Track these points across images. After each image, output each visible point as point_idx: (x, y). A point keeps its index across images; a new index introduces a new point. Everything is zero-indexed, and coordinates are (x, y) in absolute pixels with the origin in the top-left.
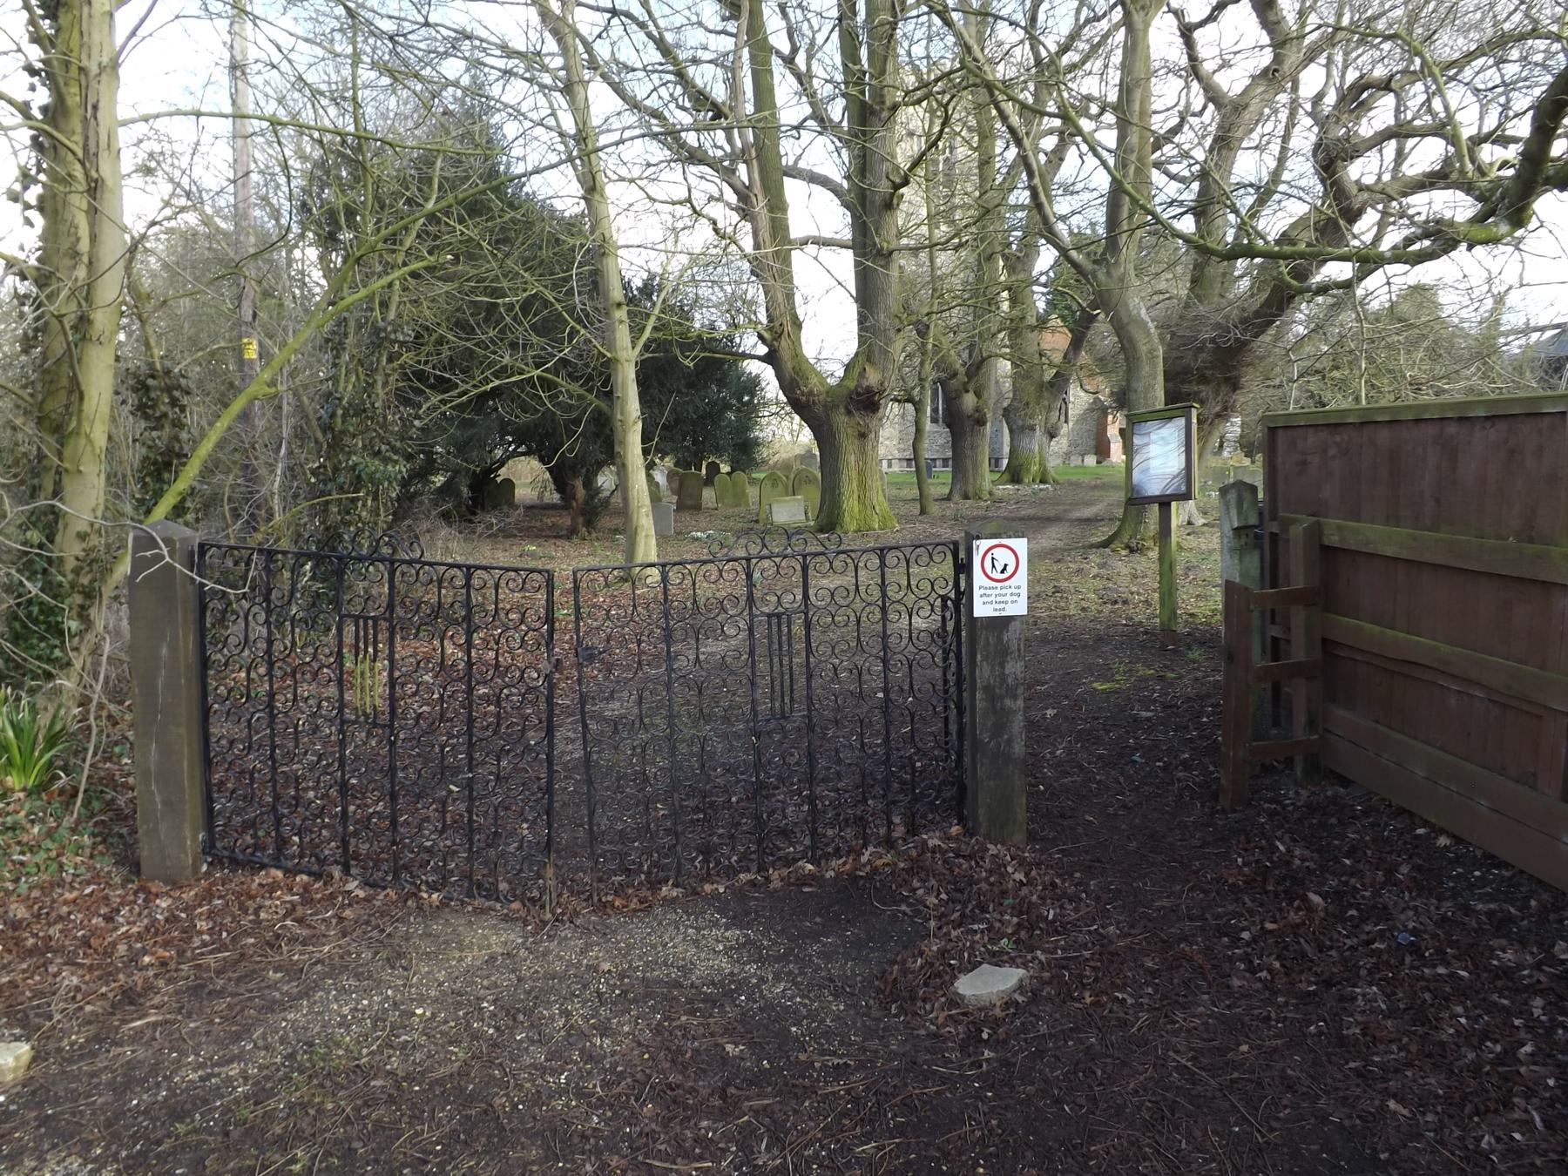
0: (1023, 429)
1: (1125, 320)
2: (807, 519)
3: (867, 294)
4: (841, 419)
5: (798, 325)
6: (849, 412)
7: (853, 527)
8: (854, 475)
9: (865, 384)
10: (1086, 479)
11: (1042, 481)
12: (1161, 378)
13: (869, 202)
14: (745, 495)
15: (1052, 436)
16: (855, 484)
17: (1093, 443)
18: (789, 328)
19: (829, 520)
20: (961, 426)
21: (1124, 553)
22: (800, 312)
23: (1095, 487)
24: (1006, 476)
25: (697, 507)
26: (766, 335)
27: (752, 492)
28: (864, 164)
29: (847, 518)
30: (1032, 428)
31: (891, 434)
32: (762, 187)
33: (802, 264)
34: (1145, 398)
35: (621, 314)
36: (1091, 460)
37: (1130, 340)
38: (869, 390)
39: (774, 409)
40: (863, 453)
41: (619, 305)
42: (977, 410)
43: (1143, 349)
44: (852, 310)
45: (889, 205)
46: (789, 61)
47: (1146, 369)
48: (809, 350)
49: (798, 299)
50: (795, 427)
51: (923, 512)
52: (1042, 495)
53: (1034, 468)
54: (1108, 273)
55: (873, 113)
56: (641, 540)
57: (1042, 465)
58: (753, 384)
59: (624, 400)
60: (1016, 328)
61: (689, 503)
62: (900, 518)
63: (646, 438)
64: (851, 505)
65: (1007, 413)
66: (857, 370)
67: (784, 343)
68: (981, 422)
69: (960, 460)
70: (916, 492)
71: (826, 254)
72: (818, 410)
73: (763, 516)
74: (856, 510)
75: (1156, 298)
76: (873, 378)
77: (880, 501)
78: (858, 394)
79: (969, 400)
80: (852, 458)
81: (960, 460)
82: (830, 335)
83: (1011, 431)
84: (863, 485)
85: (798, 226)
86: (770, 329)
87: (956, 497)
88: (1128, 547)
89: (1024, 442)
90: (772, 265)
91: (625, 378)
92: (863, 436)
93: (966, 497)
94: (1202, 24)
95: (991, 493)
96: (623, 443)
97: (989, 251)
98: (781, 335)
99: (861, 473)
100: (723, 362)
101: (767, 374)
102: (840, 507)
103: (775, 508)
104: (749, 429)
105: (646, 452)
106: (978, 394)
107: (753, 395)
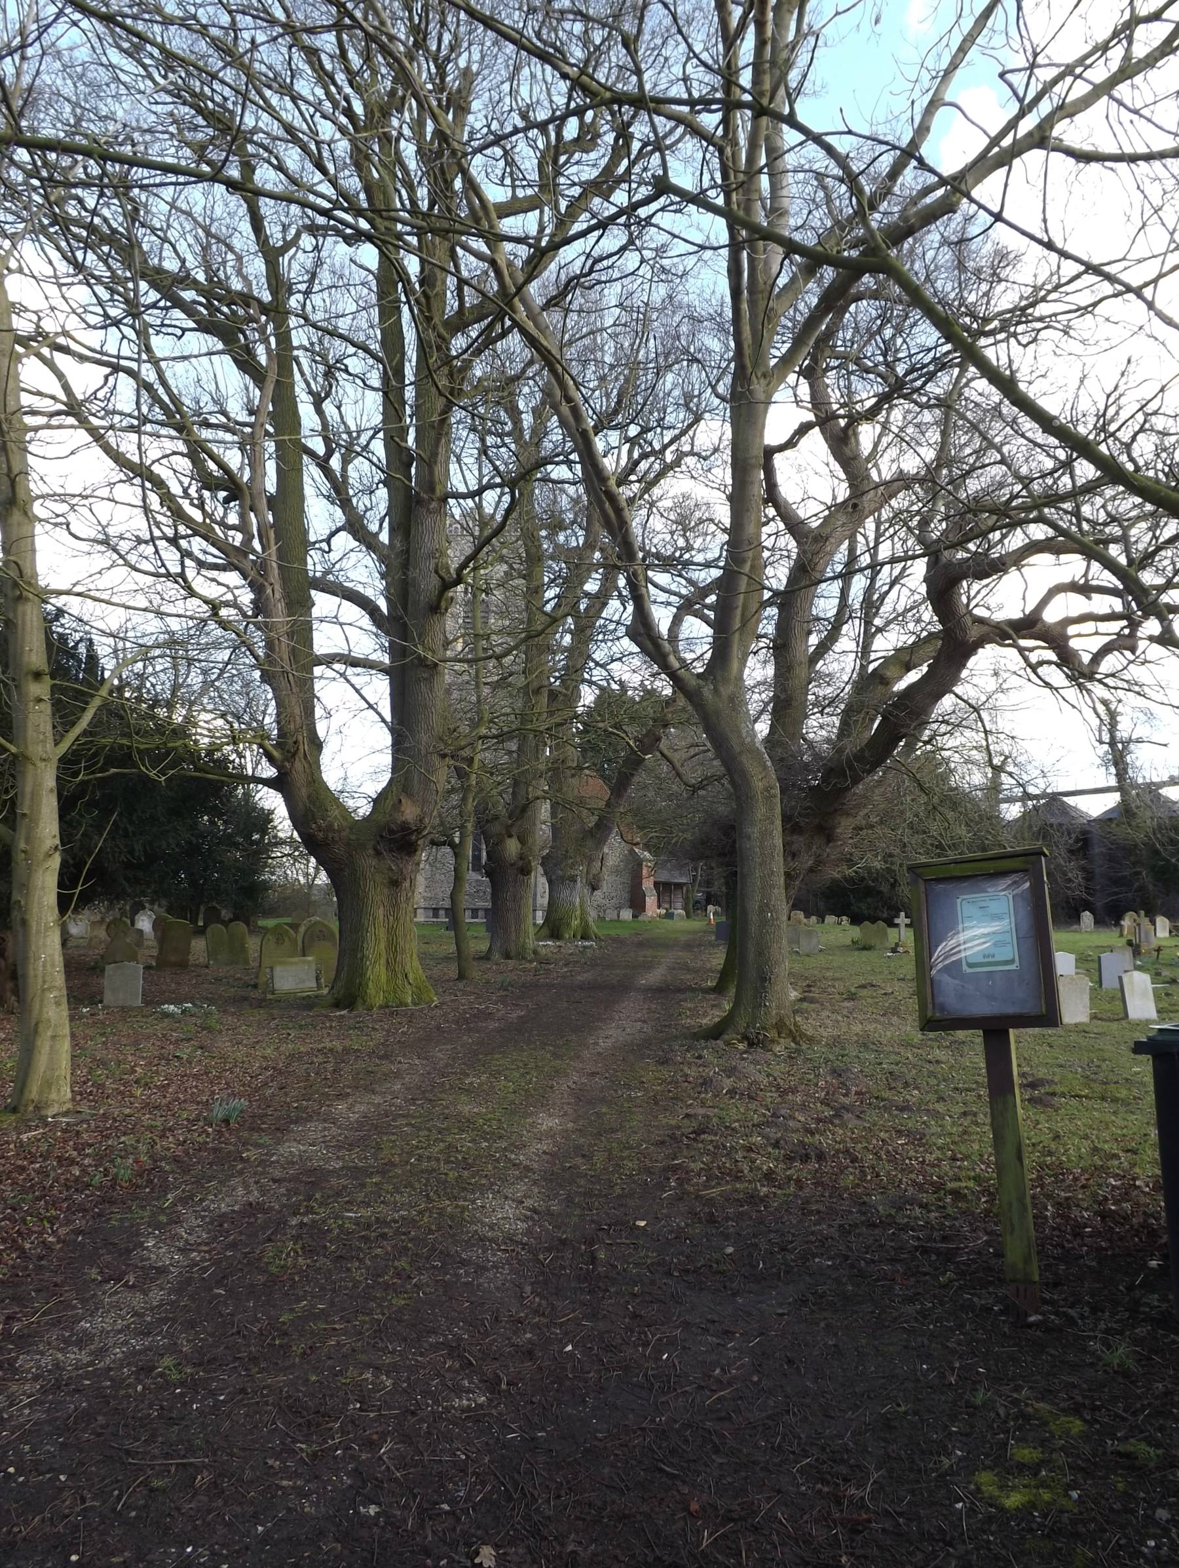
0: (562, 879)
1: (737, 749)
2: (319, 987)
3: (404, 723)
4: (367, 862)
5: (317, 745)
6: (378, 853)
7: (379, 1000)
8: (382, 934)
9: (401, 819)
10: (624, 933)
11: (584, 937)
12: (778, 823)
13: (407, 617)
14: (243, 949)
15: (594, 889)
16: (382, 946)
17: (626, 896)
18: (305, 747)
19: (347, 994)
20: (503, 876)
21: (741, 1046)
22: (321, 729)
23: (641, 945)
24: (545, 931)
25: (183, 965)
26: (276, 754)
27: (253, 944)
28: (408, 559)
29: (371, 990)
30: (573, 879)
31: (429, 878)
32: (284, 581)
33: (330, 690)
34: (762, 847)
35: (40, 689)
36: (627, 914)
37: (744, 774)
38: (405, 828)
39: (287, 850)
40: (395, 905)
41: (37, 676)
42: (521, 857)
43: (758, 784)
44: (385, 738)
45: (436, 608)
46: (323, 464)
47: (761, 811)
48: (331, 776)
49: (319, 712)
50: (311, 871)
51: (461, 976)
52: (589, 953)
53: (575, 923)
54: (716, 691)
55: (420, 502)
56: (44, 1046)
57: (583, 919)
58: (265, 819)
59: (34, 820)
60: (556, 771)
61: (173, 959)
62: (435, 982)
63: (66, 879)
64: (377, 973)
65: (545, 861)
66: (389, 803)
67: (299, 765)
68: (525, 871)
69: (500, 916)
70: (453, 948)
71: (359, 676)
72: (339, 850)
73: (262, 980)
74: (383, 978)
75: (692, 751)
76: (410, 812)
77: (414, 967)
78: (391, 832)
79: (512, 847)
80: (381, 912)
81: (500, 916)
82: (356, 755)
83: (550, 882)
84: (393, 948)
85: (325, 640)
86: (279, 745)
87: (496, 956)
88: (745, 1038)
89: (565, 894)
90: (291, 667)
91: (37, 786)
92: (395, 883)
93: (508, 956)
94: (782, 448)
95: (535, 952)
96: (25, 886)
97: (535, 685)
98: (296, 751)
99: (391, 931)
100: (223, 783)
101: (272, 801)
102: (363, 975)
103: (278, 971)
104: (259, 871)
105: (63, 904)
106: (522, 840)
107: (264, 831)
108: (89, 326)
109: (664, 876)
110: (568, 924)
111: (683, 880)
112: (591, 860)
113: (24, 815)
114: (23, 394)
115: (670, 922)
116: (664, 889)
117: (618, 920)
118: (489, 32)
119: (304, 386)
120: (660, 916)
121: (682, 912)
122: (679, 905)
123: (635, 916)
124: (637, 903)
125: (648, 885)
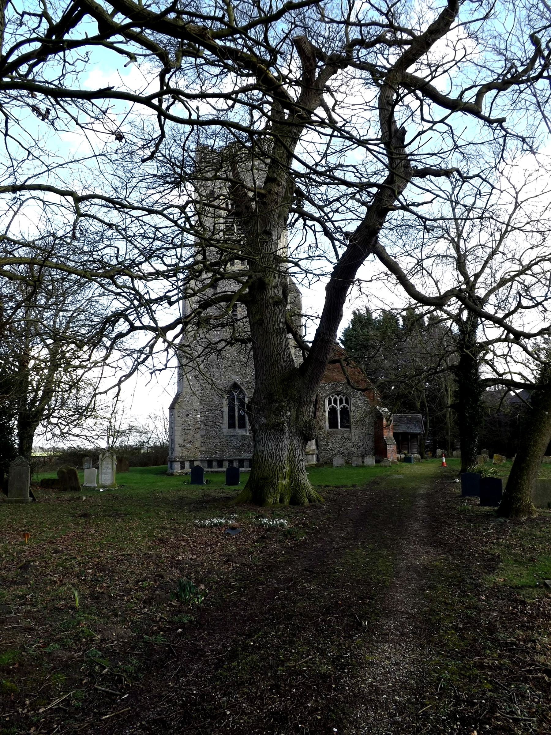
17: (372, 445)
36: (370, 461)
53: (283, 483)
57: (294, 478)
108: (354, 167)
109: (402, 428)
110: (274, 485)
111: (417, 431)
112: (300, 403)
113: (491, 457)
114: (294, 160)
115: (408, 465)
116: (403, 440)
117: (363, 466)
118: (487, 115)
119: (382, 155)
120: (399, 460)
121: (418, 456)
122: (415, 450)
123: (377, 462)
124: (380, 451)
125: (388, 435)
